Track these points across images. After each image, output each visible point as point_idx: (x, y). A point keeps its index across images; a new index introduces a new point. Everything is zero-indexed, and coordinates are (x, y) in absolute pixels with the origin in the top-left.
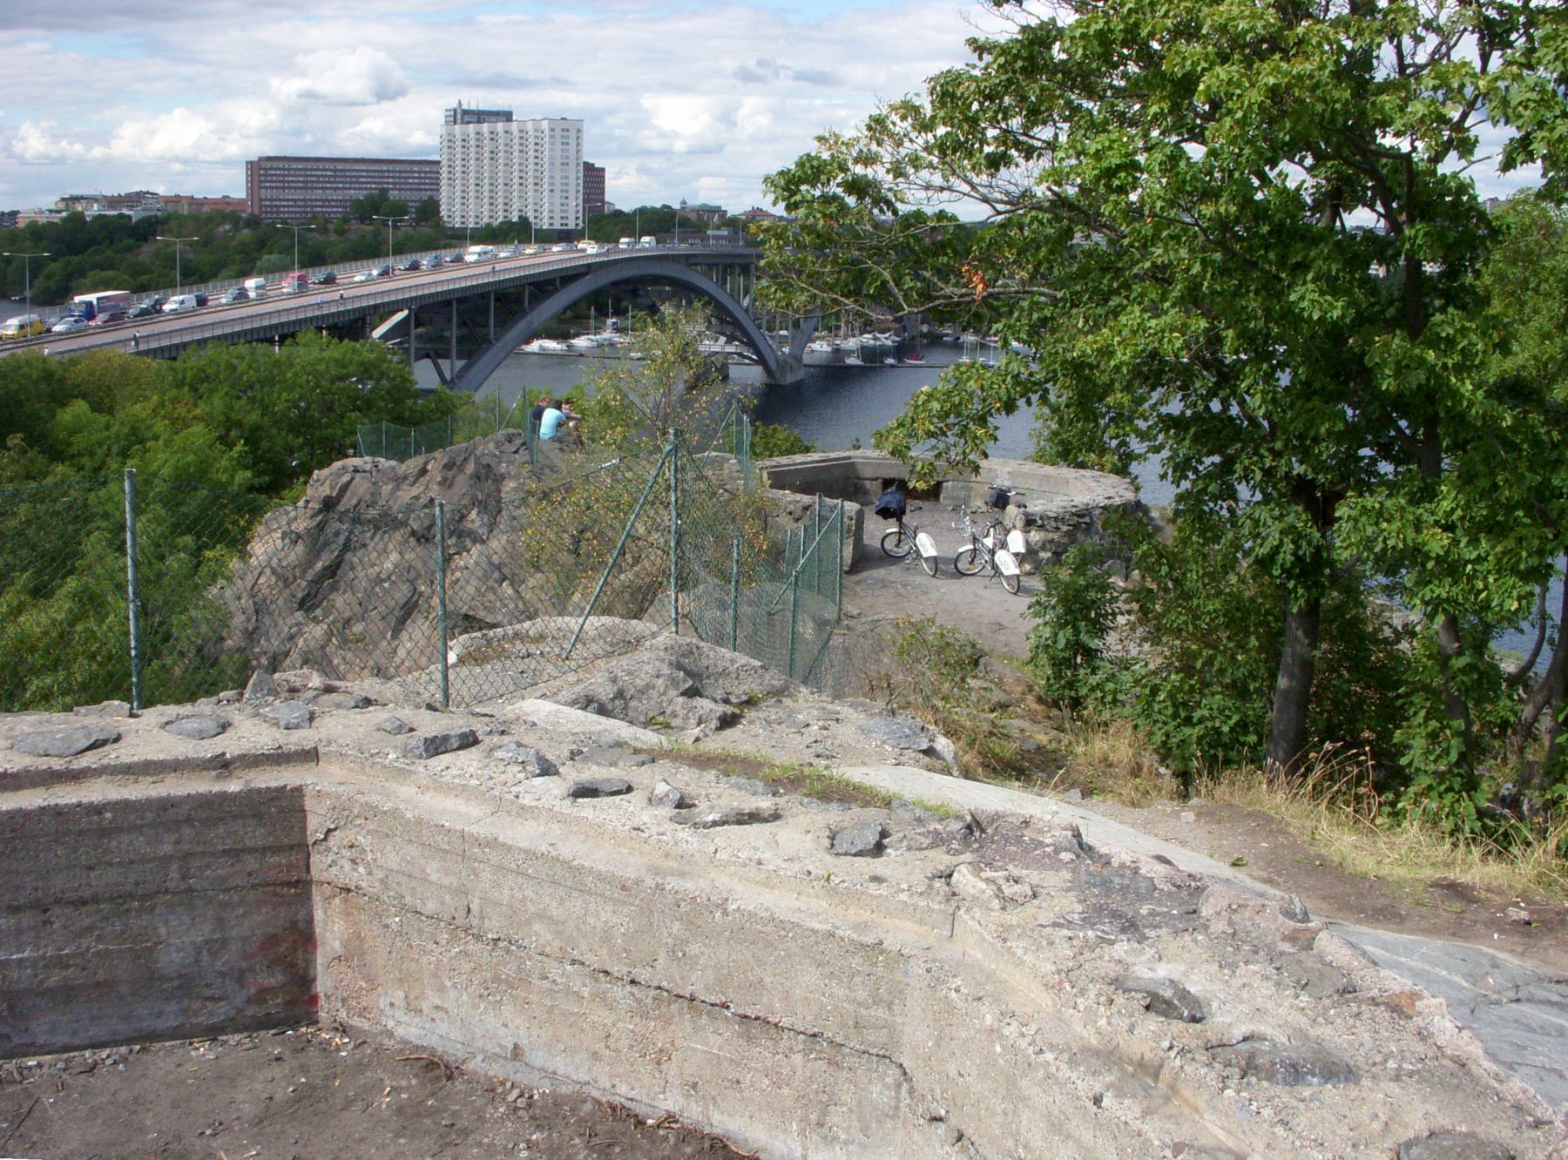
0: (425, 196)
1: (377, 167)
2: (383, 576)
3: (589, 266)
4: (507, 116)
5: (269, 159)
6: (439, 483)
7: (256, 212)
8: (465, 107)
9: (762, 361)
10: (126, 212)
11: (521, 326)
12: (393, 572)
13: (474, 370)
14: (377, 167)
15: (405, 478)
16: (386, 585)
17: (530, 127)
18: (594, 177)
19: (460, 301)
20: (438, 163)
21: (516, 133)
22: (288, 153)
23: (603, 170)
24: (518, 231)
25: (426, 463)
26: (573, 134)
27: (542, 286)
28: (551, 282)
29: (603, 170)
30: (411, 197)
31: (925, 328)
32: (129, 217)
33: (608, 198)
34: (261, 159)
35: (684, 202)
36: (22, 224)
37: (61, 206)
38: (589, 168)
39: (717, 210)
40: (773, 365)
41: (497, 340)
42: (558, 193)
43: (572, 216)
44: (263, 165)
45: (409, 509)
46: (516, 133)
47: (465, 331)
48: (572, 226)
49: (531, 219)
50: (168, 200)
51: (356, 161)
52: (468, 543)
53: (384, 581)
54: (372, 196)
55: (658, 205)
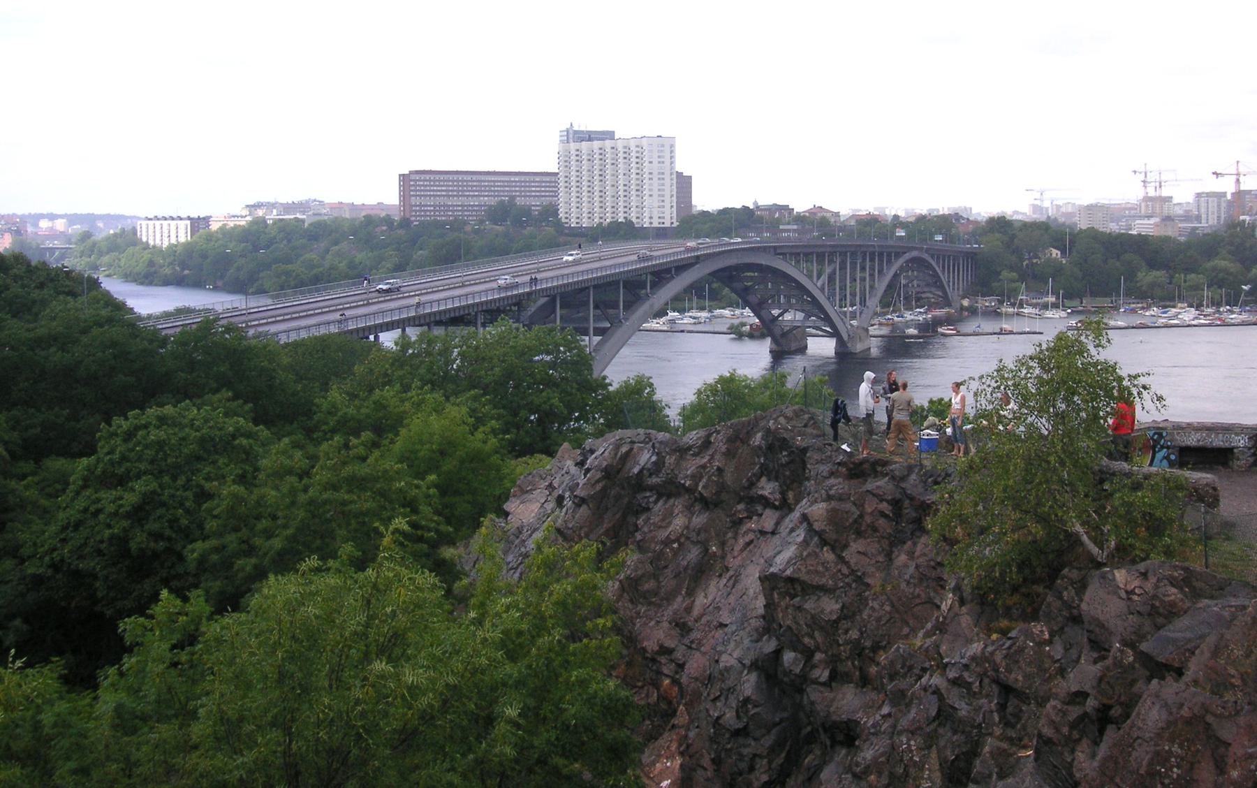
0: (546, 201)
1: (506, 178)
2: (673, 538)
3: (698, 257)
4: (609, 135)
5: (417, 172)
6: (724, 454)
7: (408, 216)
8: (576, 128)
9: (835, 334)
10: (299, 216)
11: (644, 308)
12: (682, 535)
13: (608, 344)
14: (506, 178)
15: (689, 448)
16: (675, 545)
17: (632, 144)
18: (684, 183)
19: (595, 287)
20: (556, 174)
21: (621, 149)
22: (459, 169)
23: (404, 179)
24: (624, 231)
25: (710, 435)
26: (667, 149)
27: (661, 275)
28: (668, 271)
29: (404, 179)
30: (536, 204)
31: (966, 303)
32: (303, 221)
33: (694, 203)
34: (411, 173)
35: (755, 203)
36: (214, 226)
37: (245, 212)
38: (679, 175)
39: (786, 208)
40: (845, 337)
41: (626, 319)
42: (655, 197)
43: (668, 217)
44: (413, 177)
45: (696, 477)
46: (621, 149)
47: (598, 312)
48: (667, 225)
49: (634, 220)
50: (333, 207)
51: (488, 173)
52: (759, 508)
53: (674, 541)
54: (502, 202)
55: (739, 206)
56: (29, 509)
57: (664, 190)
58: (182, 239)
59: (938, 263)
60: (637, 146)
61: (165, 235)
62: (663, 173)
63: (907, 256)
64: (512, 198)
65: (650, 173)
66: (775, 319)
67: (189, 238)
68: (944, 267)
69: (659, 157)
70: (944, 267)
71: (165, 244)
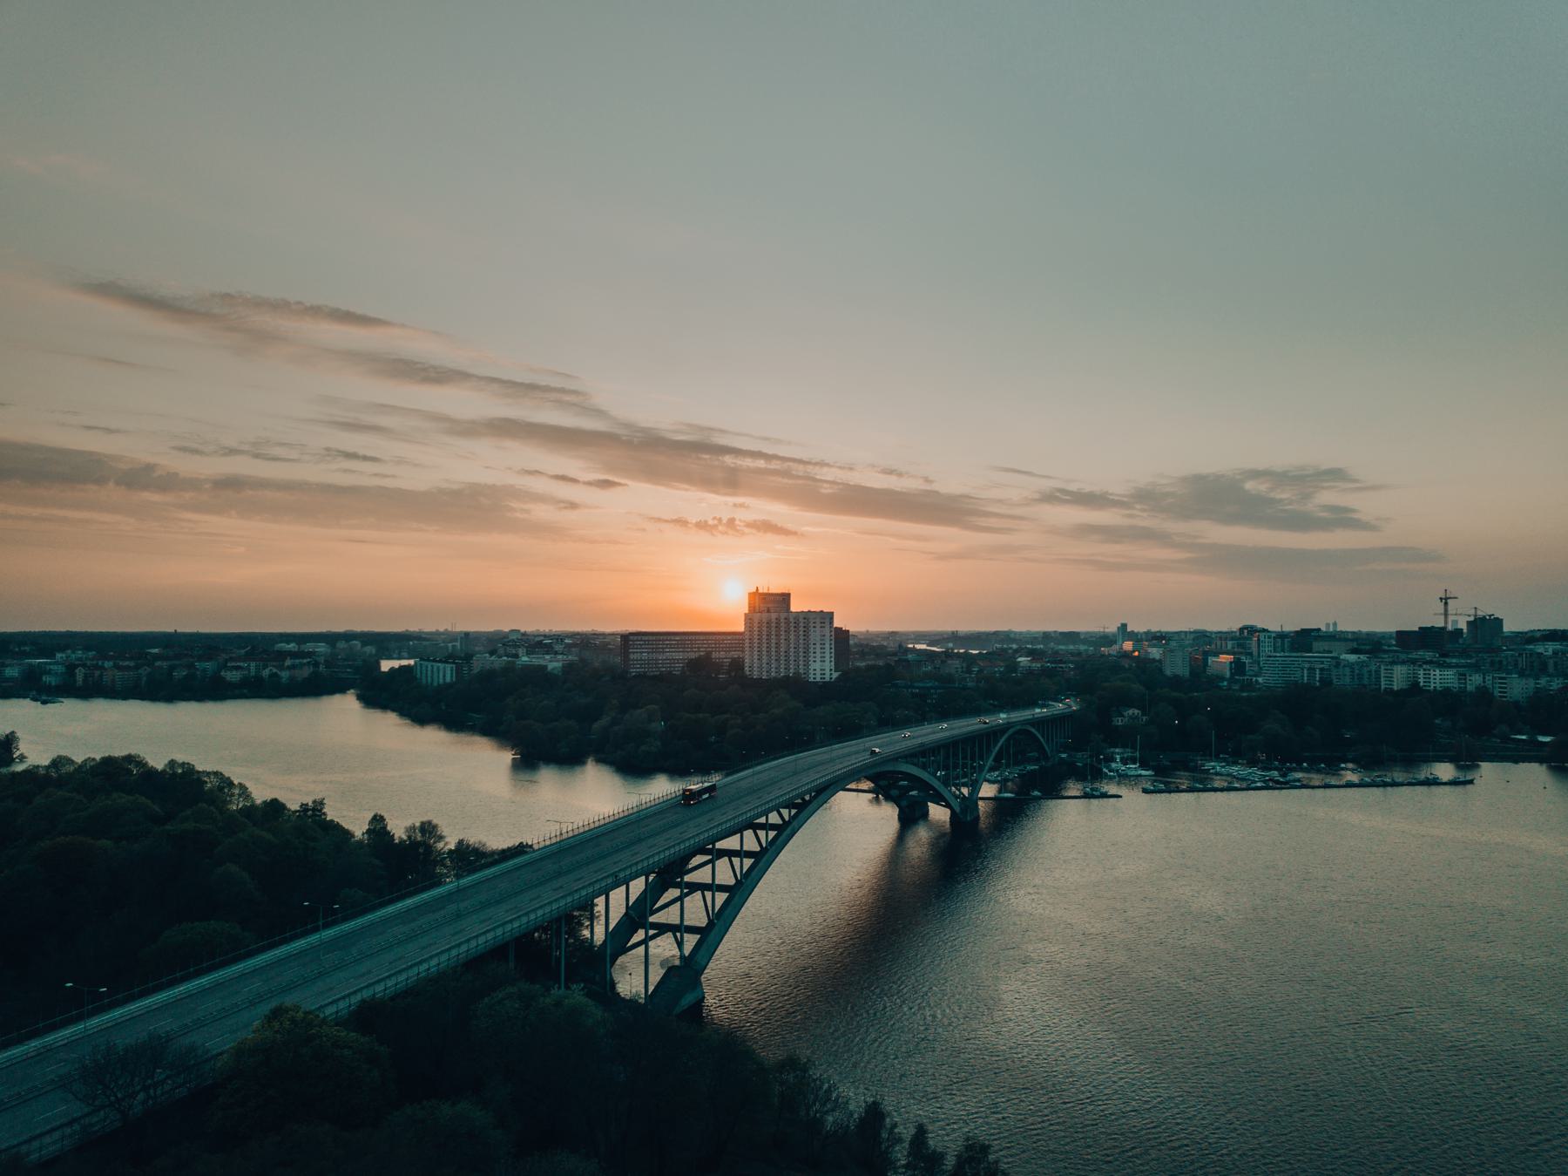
0: (735, 654)
8: (761, 591)
38: (839, 630)
43: (828, 672)
46: (791, 620)
56: (294, 1014)
57: (824, 657)
58: (448, 679)
59: (1043, 737)
60: (805, 619)
61: (441, 676)
62: (824, 670)
63: (1011, 731)
64: (709, 654)
65: (814, 644)
66: (582, 925)
67: (454, 679)
68: (1048, 740)
69: (824, 653)
70: (1048, 740)
71: (435, 684)
